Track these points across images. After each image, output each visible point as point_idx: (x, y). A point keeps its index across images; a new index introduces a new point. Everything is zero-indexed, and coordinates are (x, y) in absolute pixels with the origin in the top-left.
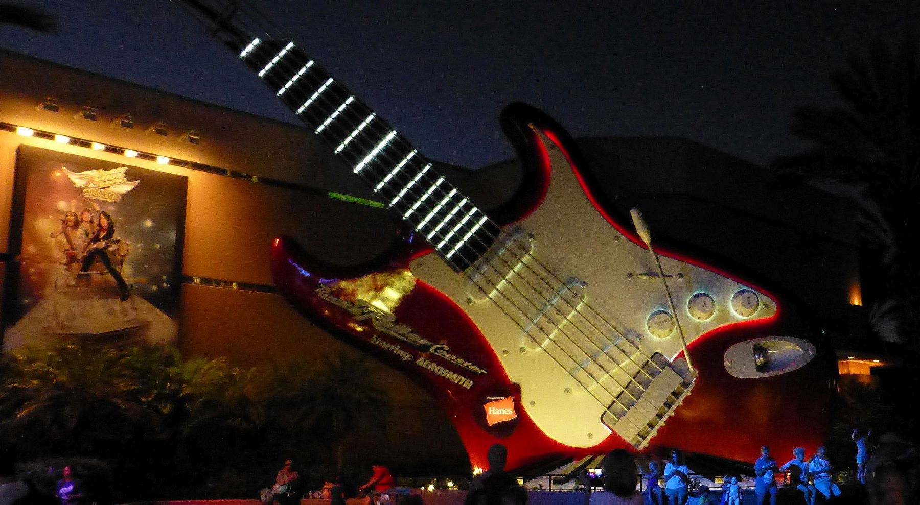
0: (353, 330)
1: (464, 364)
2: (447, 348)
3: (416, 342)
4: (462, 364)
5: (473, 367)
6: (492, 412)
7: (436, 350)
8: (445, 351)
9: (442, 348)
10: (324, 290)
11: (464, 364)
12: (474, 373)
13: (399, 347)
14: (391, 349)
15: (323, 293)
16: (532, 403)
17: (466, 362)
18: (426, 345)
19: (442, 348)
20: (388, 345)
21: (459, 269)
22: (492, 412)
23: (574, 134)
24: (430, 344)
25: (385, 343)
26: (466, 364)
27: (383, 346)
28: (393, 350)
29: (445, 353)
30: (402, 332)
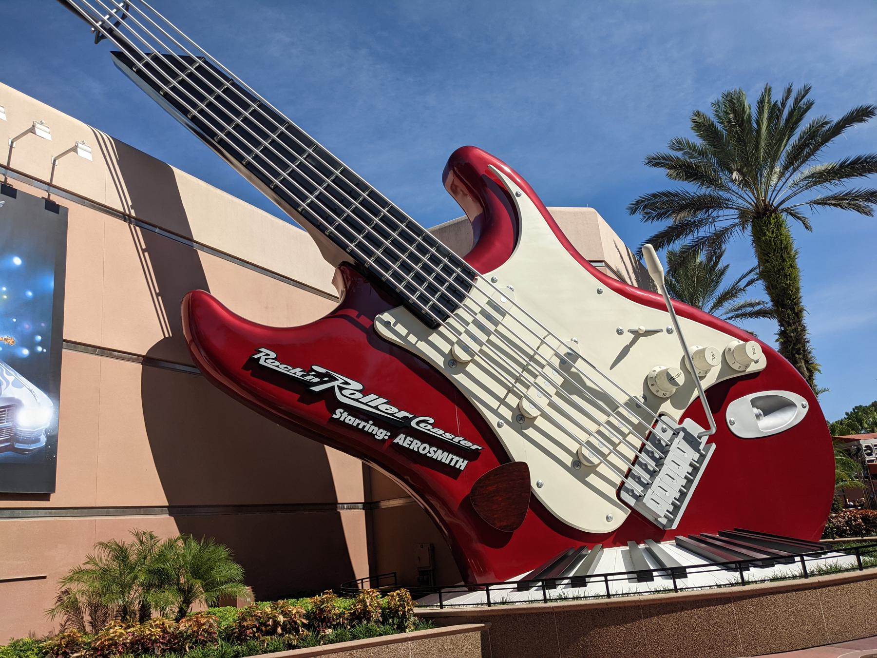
1: (453, 440)
2: (431, 421)
4: (451, 440)
5: (466, 442)
7: (418, 423)
11: (453, 440)
13: (371, 422)
14: (360, 427)
15: (266, 359)
18: (406, 417)
20: (358, 421)
24: (410, 416)
26: (457, 439)
27: (351, 423)
28: (364, 427)
29: (430, 427)
30: (373, 404)
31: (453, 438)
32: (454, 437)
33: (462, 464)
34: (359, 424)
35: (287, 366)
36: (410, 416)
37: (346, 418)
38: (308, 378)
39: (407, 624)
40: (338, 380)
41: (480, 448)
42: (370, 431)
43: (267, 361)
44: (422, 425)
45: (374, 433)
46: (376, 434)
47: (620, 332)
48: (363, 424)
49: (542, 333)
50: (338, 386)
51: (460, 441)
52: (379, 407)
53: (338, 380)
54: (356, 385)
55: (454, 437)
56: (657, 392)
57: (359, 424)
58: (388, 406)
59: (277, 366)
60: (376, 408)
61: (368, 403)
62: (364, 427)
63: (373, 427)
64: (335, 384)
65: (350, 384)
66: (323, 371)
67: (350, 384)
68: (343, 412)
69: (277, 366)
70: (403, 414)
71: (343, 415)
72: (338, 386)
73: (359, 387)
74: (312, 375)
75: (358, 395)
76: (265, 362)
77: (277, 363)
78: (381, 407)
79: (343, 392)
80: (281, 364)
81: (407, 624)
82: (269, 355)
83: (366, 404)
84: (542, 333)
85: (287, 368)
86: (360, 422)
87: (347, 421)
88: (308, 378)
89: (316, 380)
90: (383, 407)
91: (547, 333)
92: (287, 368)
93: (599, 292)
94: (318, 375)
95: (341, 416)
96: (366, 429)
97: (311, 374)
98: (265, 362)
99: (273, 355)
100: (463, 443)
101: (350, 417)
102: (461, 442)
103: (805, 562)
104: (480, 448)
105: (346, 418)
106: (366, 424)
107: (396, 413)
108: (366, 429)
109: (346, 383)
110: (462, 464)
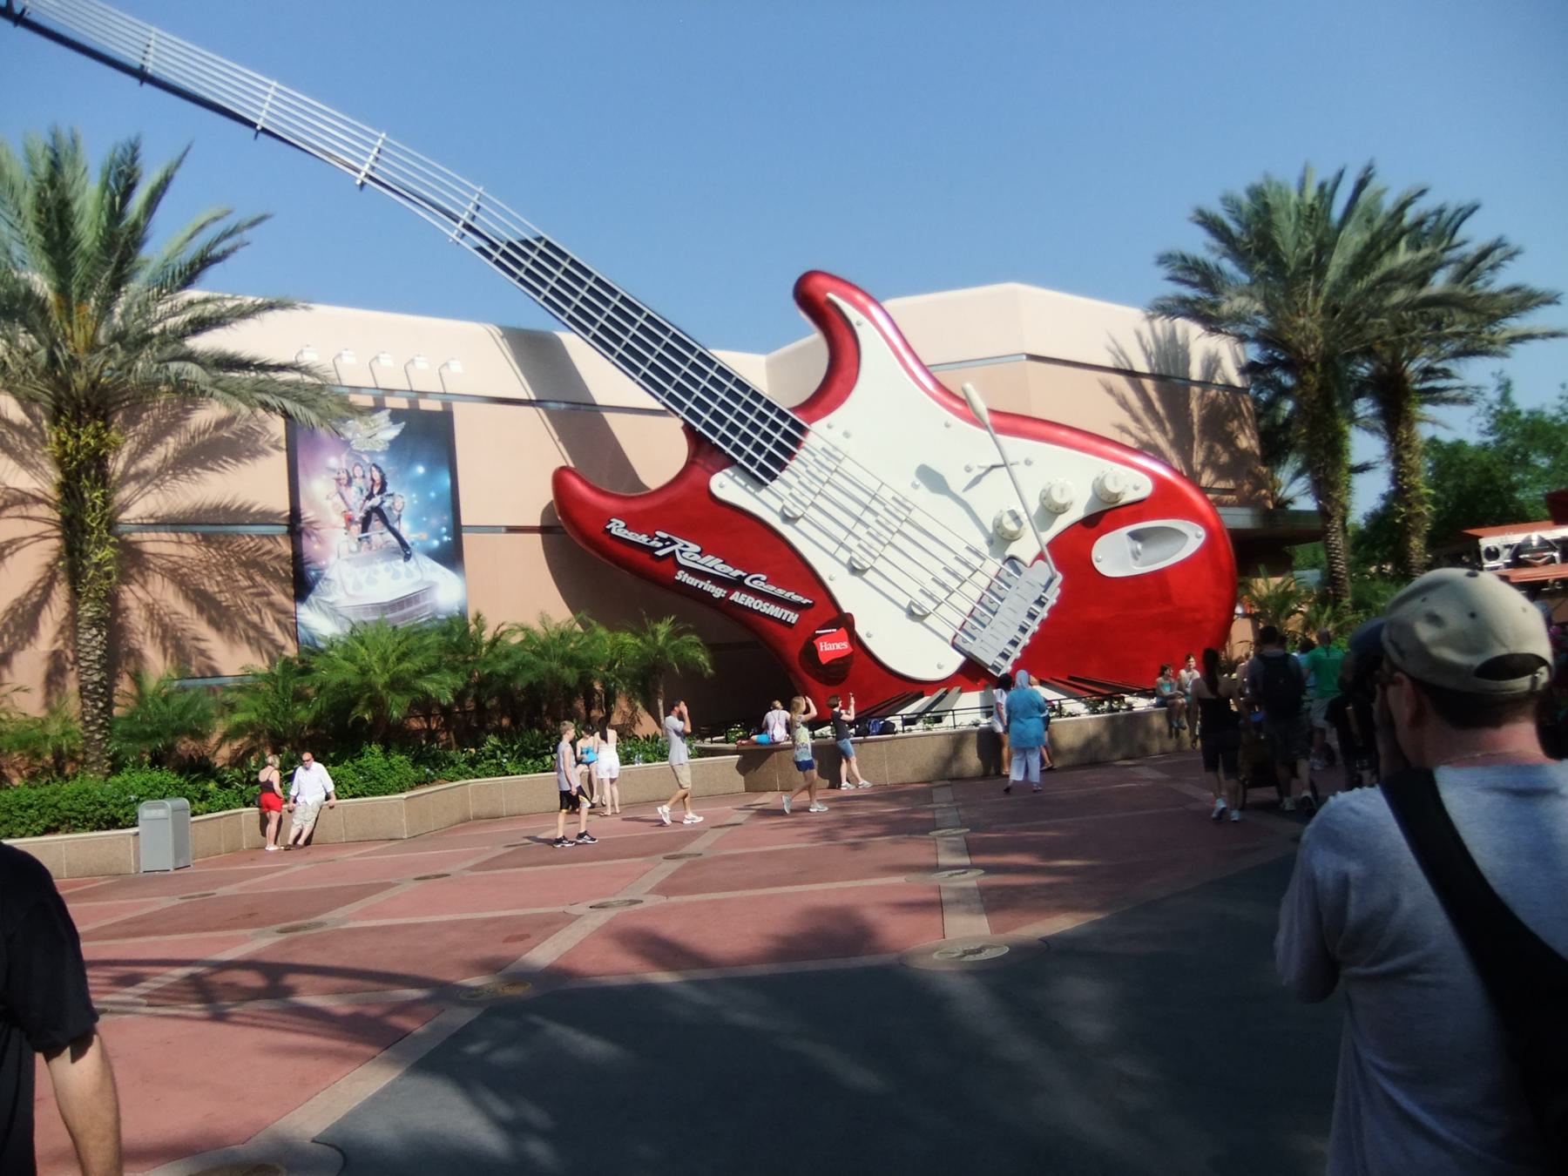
2: (764, 577)
7: (751, 581)
18: (740, 576)
20: (697, 581)
24: (744, 574)
29: (763, 584)
30: (710, 565)
58: (724, 566)
63: (711, 586)
73: (698, 549)
75: (697, 557)
77: (626, 531)
83: (713, 568)
89: (660, 544)
94: (661, 540)
109: (685, 546)
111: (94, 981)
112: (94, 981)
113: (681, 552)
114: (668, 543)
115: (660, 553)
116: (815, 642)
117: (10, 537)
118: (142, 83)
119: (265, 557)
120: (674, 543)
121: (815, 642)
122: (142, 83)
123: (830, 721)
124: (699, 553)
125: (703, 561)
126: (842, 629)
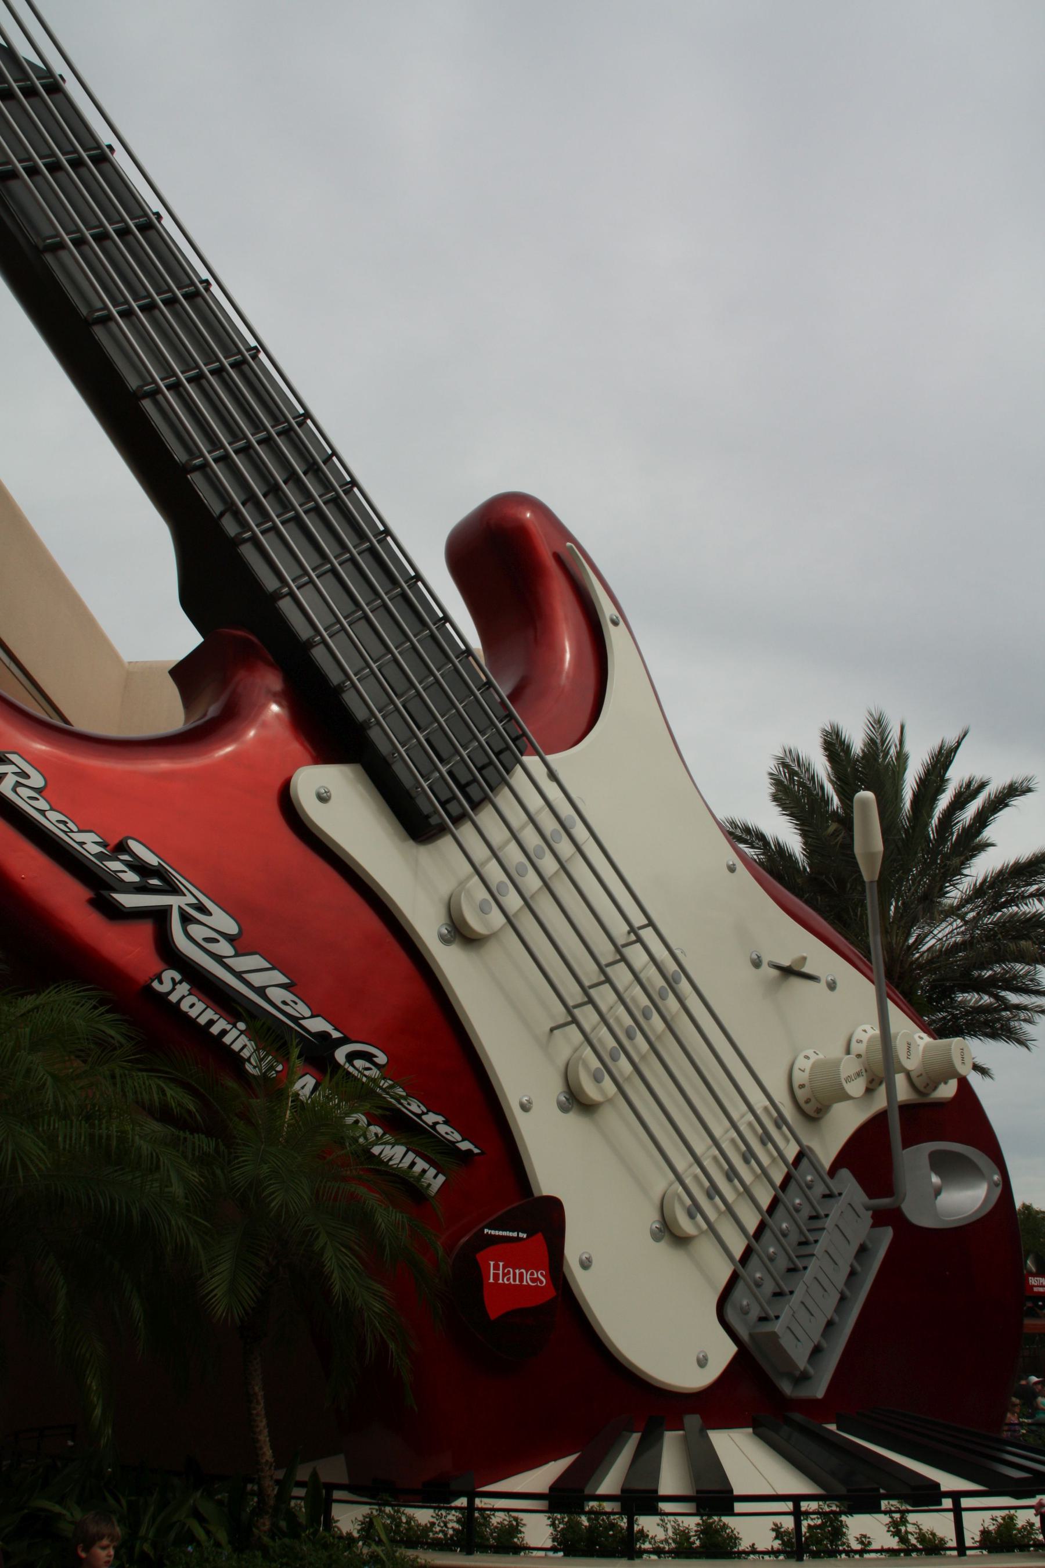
0: (808, 808)
1: (424, 1117)
2: (382, 1058)
3: (295, 1020)
4: (419, 1116)
5: (448, 1129)
6: (496, 1276)
7: (351, 1057)
8: (376, 1065)
9: (368, 1057)
10: (25, 775)
11: (424, 1117)
12: (450, 1148)
13: (241, 1026)
14: (215, 1030)
15: (18, 784)
16: (586, 1265)
17: (429, 1111)
18: (324, 1036)
19: (368, 1057)
20: (210, 1014)
21: (889, 756)
22: (496, 1276)
23: (13, 766)
24: (336, 1034)
25: (200, 1006)
26: (431, 1118)
27: (193, 1013)
28: (224, 1032)
29: (374, 1073)
30: (256, 979)
31: (424, 1113)
32: (425, 1110)
33: (435, 1181)
34: (211, 1023)
35: (64, 818)
36: (336, 1034)
37: (183, 997)
38: (114, 866)
39: (124, 1503)
40: (185, 895)
41: (476, 1151)
42: (236, 1047)
43: (19, 790)
44: (359, 1063)
45: (246, 1054)
46: (249, 1060)
47: (757, 963)
48: (221, 1025)
49: (638, 920)
50: (180, 907)
51: (438, 1123)
52: (269, 991)
53: (185, 895)
54: (223, 921)
55: (425, 1110)
56: (525, 1108)
57: (211, 1023)
58: (288, 996)
59: (42, 812)
60: (261, 991)
61: (244, 975)
62: (224, 1032)
63: (243, 1040)
64: (173, 901)
65: (210, 914)
66: (152, 860)
67: (210, 914)
68: (180, 982)
69: (42, 812)
70: (318, 1025)
71: (178, 987)
72: (180, 907)
73: (231, 927)
74: (123, 861)
75: (224, 948)
76: (14, 790)
77: (42, 804)
78: (271, 992)
79: (192, 929)
80: (52, 809)
81: (124, 1503)
82: (28, 777)
83: (239, 975)
84: (638, 920)
85: (65, 823)
86: (216, 1017)
87: (184, 1006)
88: (114, 866)
89: (131, 877)
90: (277, 995)
91: (646, 922)
92: (65, 823)
93: (732, 869)
94: (139, 867)
95: (173, 989)
96: (227, 1040)
97: (122, 857)
98: (14, 790)
99: (37, 780)
100: (443, 1129)
101: (192, 999)
102: (438, 1127)
103: (964, 1513)
104: (476, 1151)
105: (183, 997)
106: (228, 1027)
107: (304, 1018)
108: (227, 1040)
109: (201, 908)
110: (432, 1181)
111: (497, 833)
112: (497, 833)
113: (186, 919)
114: (154, 882)
115: (129, 901)
116: (479, 1256)
117: (894, 1560)
118: (882, 1547)
119: (1022, 967)
120: (173, 890)
121: (479, 1256)
122: (882, 1547)
123: (914, 830)
124: (231, 939)
125: (242, 963)
126: (540, 1236)
